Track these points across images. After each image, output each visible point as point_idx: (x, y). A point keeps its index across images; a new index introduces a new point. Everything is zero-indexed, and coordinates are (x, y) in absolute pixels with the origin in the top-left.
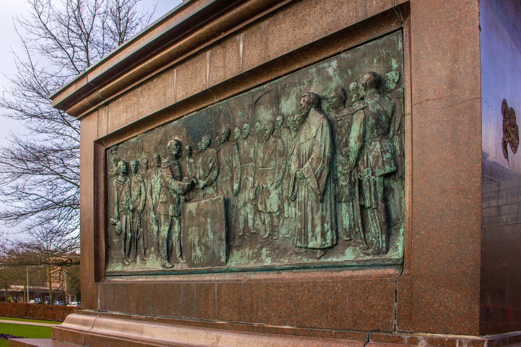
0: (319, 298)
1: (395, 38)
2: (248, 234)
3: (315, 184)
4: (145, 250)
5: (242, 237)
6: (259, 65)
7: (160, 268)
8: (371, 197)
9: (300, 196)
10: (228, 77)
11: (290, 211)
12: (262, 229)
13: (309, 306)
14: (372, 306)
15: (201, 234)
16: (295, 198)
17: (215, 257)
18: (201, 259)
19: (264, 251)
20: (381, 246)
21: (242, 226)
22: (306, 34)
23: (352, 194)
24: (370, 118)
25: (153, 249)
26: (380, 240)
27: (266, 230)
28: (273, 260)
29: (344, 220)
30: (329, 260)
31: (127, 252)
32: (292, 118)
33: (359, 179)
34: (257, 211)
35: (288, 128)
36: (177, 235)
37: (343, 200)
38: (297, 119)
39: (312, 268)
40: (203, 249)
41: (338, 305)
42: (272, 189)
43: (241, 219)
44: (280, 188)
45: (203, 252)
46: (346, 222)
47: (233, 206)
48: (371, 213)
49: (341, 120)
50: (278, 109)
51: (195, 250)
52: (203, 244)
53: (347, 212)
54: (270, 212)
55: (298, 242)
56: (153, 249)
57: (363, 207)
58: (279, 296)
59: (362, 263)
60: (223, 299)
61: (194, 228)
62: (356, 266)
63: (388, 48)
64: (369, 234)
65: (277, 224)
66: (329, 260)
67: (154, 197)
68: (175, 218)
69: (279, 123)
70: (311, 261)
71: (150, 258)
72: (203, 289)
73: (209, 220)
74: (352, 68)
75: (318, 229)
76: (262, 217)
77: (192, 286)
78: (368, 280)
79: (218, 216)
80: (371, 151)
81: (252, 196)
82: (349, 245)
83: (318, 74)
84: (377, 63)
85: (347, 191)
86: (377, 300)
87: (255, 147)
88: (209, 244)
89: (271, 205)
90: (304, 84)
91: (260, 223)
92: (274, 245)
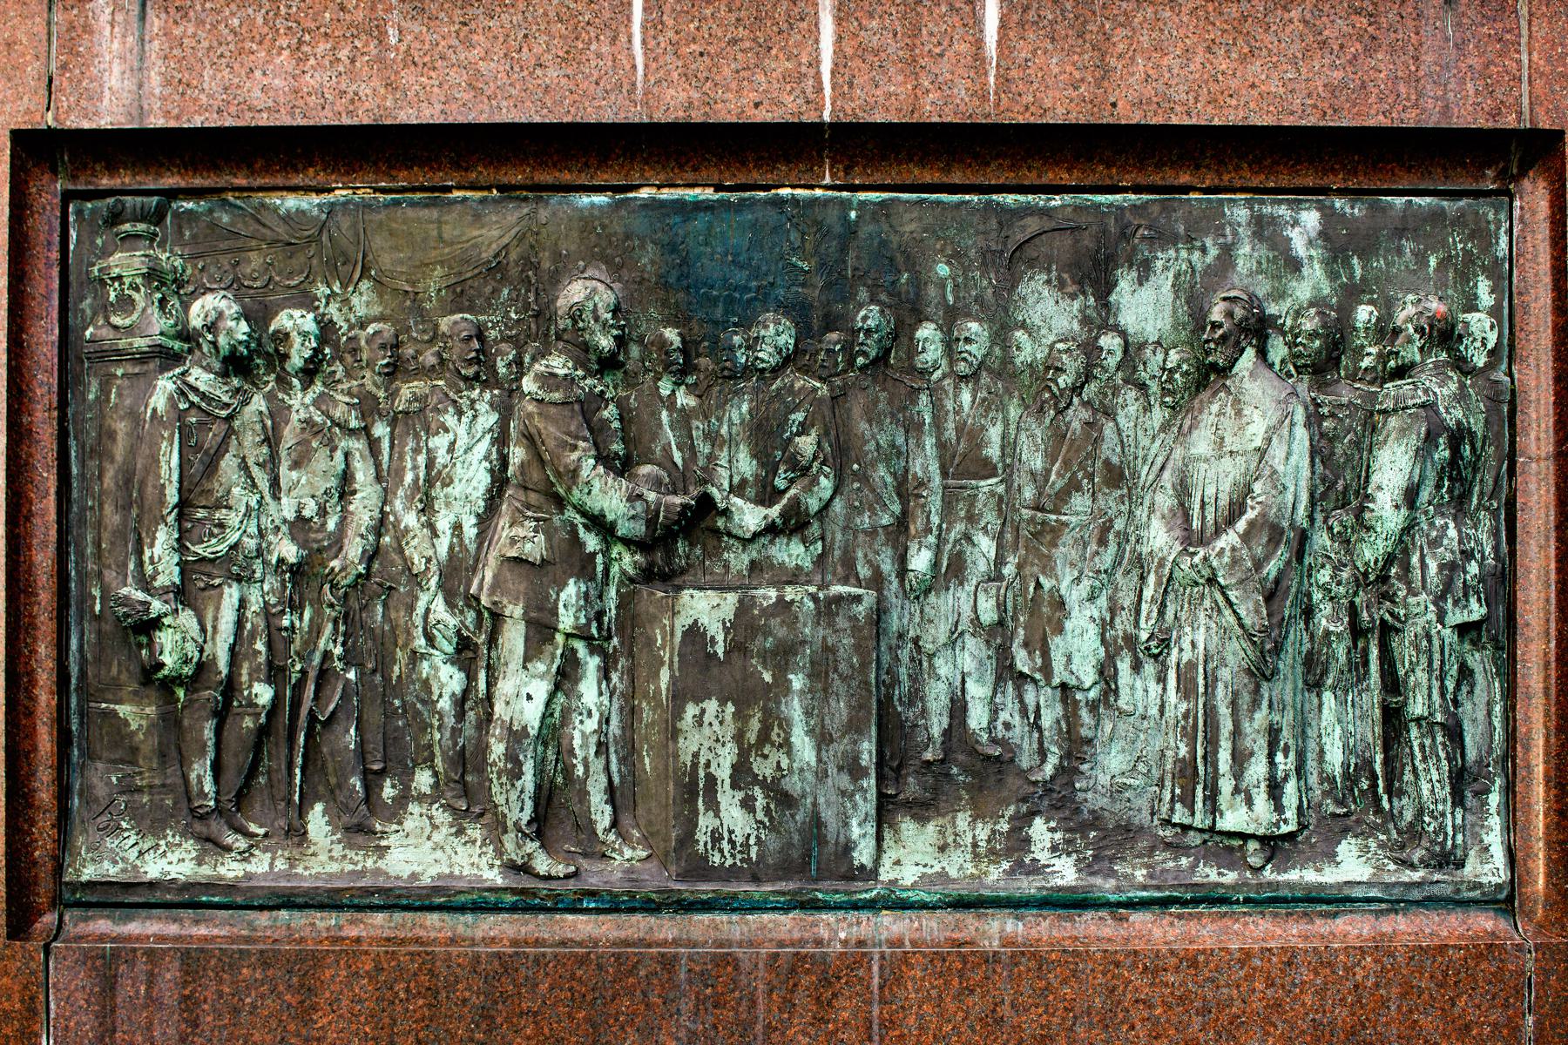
0: (1304, 1004)
1: (1491, 216)
2: (961, 757)
3: (1257, 611)
4: (371, 782)
5: (937, 771)
6: (1073, 119)
7: (494, 877)
8: (1430, 688)
9: (1186, 645)
10: (931, 110)
11: (1139, 693)
12: (1026, 746)
13: (1267, 1033)
14: (1468, 1027)
15: (752, 737)
16: (1165, 643)
17: (822, 840)
18: (746, 845)
19: (1040, 830)
20: (1449, 843)
21: (937, 725)
22: (1253, 86)
24: (1441, 441)
25: (423, 780)
26: (1450, 824)
27: (1043, 753)
28: (1085, 867)
29: (1327, 748)
30: (1293, 875)
31: (233, 780)
32: (1160, 357)
33: (1382, 620)
34: (1005, 672)
35: (1142, 387)
36: (591, 725)
37: (1330, 682)
38: (1179, 366)
39: (1237, 902)
40: (760, 802)
41: (1364, 1028)
42: (1074, 595)
43: (937, 696)
44: (1103, 601)
45: (760, 815)
46: (1335, 758)
47: (901, 636)
48: (1423, 736)
49: (1333, 415)
50: (1105, 305)
51: (713, 806)
52: (763, 784)
53: (1339, 721)
54: (1064, 686)
55: (1178, 806)
56: (423, 780)
58: (1157, 1000)
59: (1397, 893)
60: (912, 1020)
61: (712, 706)
62: (1380, 901)
63: (1471, 237)
64: (1405, 801)
65: (1090, 734)
66: (1293, 875)
67: (443, 523)
68: (580, 647)
69: (1112, 362)
70: (1231, 877)
71: (409, 824)
72: (805, 981)
73: (797, 682)
74: (1365, 256)
75: (1257, 769)
76: (1030, 697)
77: (746, 965)
78: (1455, 947)
79: (843, 667)
80: (1435, 543)
82: (1345, 831)
83: (1254, 233)
84: (1436, 270)
85: (1341, 650)
86: (1479, 1007)
87: (1006, 424)
88: (793, 785)
89: (1069, 658)
90: (1204, 250)
91: (1017, 720)
92: (1077, 811)
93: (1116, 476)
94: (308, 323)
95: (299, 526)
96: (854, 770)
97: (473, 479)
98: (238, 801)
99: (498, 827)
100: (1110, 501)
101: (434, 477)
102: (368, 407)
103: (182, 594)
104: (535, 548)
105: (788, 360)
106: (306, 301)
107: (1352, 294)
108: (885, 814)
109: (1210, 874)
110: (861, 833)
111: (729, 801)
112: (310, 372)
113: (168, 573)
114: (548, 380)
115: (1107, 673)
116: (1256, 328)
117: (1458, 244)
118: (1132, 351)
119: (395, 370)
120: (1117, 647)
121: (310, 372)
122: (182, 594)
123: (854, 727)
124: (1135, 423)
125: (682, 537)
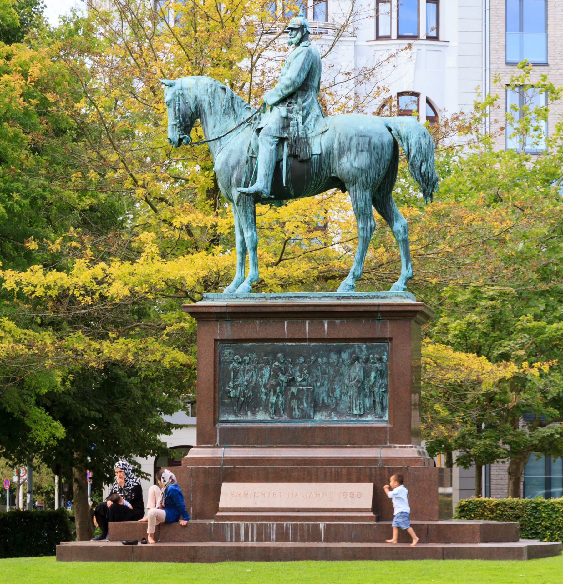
21: (321, 402)
23: (370, 395)
34: (329, 396)
43: (321, 399)
46: (368, 405)
57: (374, 401)
75: (358, 407)
81: (327, 389)
93: (342, 374)
94: (248, 358)
95: (247, 381)
96: (311, 407)
97: (267, 375)
98: (240, 410)
99: (270, 413)
100: (341, 377)
101: (263, 375)
102: (255, 367)
103: (233, 388)
104: (274, 383)
105: (303, 362)
106: (248, 356)
107: (370, 354)
108: (315, 412)
109: (352, 419)
110: (312, 414)
111: (297, 411)
112: (248, 364)
113: (232, 386)
114: (276, 365)
115: (341, 396)
116: (357, 359)
117: (382, 348)
118: (343, 361)
119: (258, 363)
120: (342, 393)
121: (248, 364)
122: (233, 388)
123: (311, 402)
124: (344, 369)
125: (291, 382)
